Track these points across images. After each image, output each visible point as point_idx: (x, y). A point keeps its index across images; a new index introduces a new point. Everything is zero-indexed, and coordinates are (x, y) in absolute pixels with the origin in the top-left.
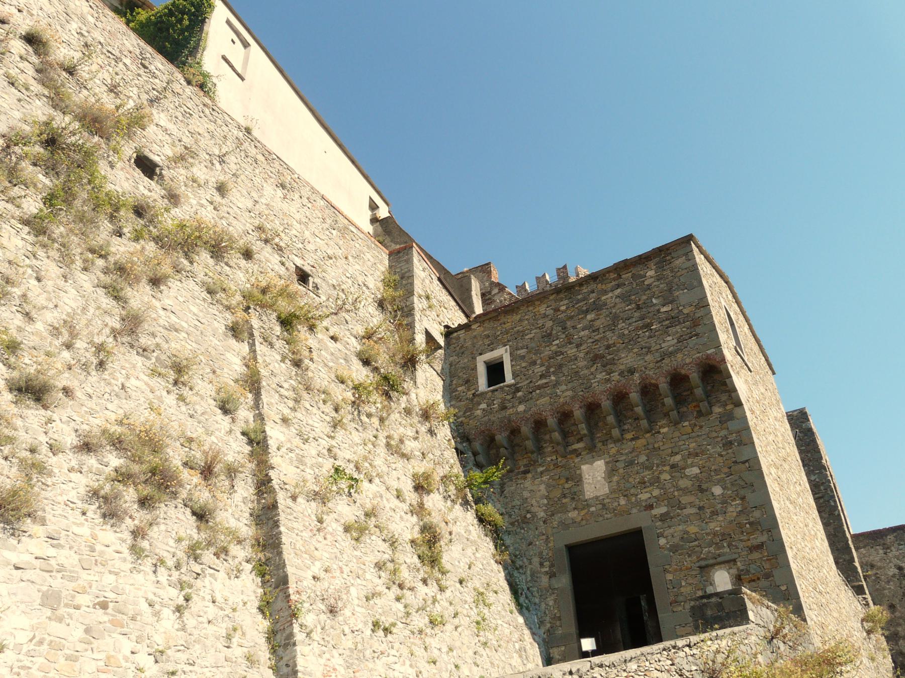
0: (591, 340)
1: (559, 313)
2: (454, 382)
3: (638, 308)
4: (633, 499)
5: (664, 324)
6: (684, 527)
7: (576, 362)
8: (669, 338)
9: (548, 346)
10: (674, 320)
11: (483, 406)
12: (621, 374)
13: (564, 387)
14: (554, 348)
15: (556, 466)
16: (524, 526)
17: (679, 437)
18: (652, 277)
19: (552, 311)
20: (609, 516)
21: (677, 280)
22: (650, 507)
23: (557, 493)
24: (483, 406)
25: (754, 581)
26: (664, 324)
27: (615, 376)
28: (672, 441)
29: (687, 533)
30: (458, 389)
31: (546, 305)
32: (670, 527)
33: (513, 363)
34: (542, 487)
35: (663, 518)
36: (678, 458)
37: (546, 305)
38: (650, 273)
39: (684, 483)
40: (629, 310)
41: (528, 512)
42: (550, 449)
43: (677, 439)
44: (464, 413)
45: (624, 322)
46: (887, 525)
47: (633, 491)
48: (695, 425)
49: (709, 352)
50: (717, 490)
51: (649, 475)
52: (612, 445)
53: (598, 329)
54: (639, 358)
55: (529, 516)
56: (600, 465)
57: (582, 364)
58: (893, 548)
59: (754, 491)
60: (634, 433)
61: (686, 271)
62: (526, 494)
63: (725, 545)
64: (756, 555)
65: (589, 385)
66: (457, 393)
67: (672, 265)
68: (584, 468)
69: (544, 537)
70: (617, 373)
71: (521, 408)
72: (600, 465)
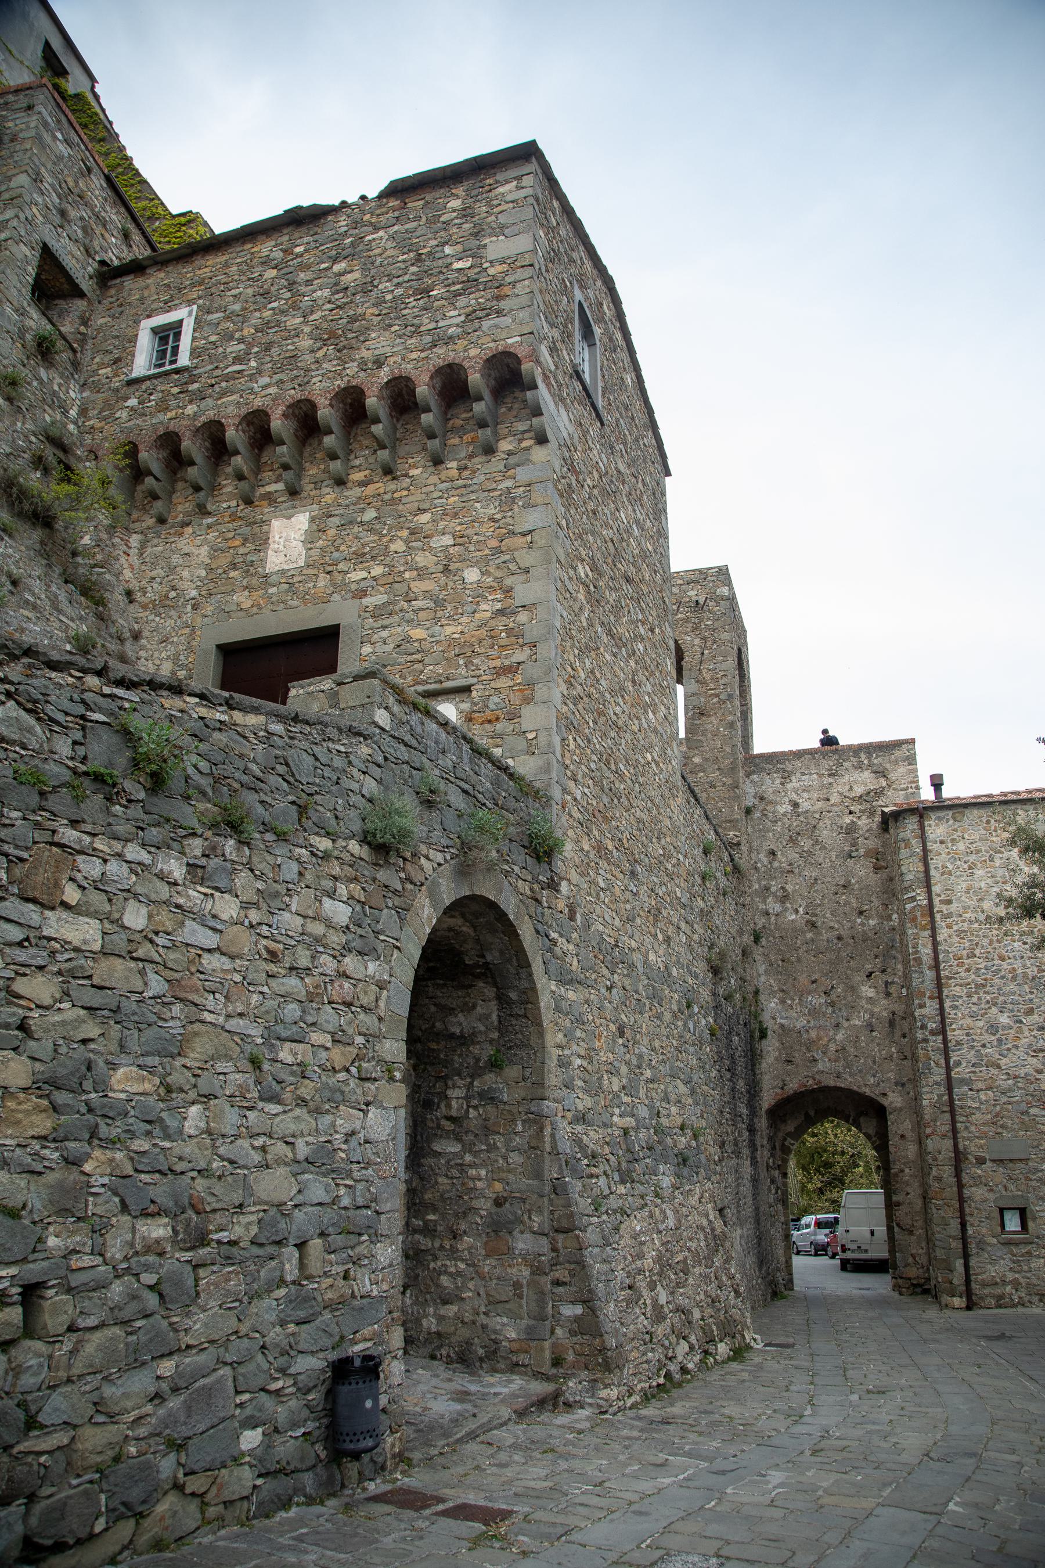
0: (329, 306)
1: (291, 257)
2: (97, 360)
3: (419, 259)
4: (339, 578)
5: (452, 289)
6: (407, 629)
7: (296, 340)
8: (453, 313)
9: (259, 310)
10: (470, 284)
11: (133, 402)
12: (363, 366)
13: (266, 380)
14: (267, 314)
15: (234, 518)
16: (162, 610)
17: (435, 485)
18: (454, 211)
19: (281, 254)
20: (295, 603)
21: (493, 218)
22: (362, 593)
23: (224, 560)
24: (133, 402)
25: (490, 722)
26: (452, 289)
27: (352, 368)
28: (424, 490)
29: (408, 639)
30: (100, 372)
31: (273, 243)
32: (384, 627)
33: (196, 335)
34: (204, 550)
35: (377, 613)
36: (425, 518)
37: (273, 243)
38: (455, 204)
39: (422, 559)
40: (404, 261)
41: (173, 588)
42: (229, 489)
43: (432, 488)
44: (100, 413)
45: (389, 280)
46: (795, 747)
47: (342, 566)
48: (466, 468)
49: (510, 341)
50: (472, 575)
51: (372, 542)
52: (328, 490)
53: (346, 288)
54: (397, 341)
55: (173, 594)
56: (302, 521)
57: (306, 343)
58: (793, 778)
59: (528, 581)
60: (367, 472)
61: (511, 205)
62: (176, 560)
63: (461, 662)
64: (503, 682)
65: (306, 380)
66: (97, 378)
67: (492, 195)
68: (276, 523)
69: (187, 631)
70: (356, 364)
71: (191, 410)
72: (302, 521)
